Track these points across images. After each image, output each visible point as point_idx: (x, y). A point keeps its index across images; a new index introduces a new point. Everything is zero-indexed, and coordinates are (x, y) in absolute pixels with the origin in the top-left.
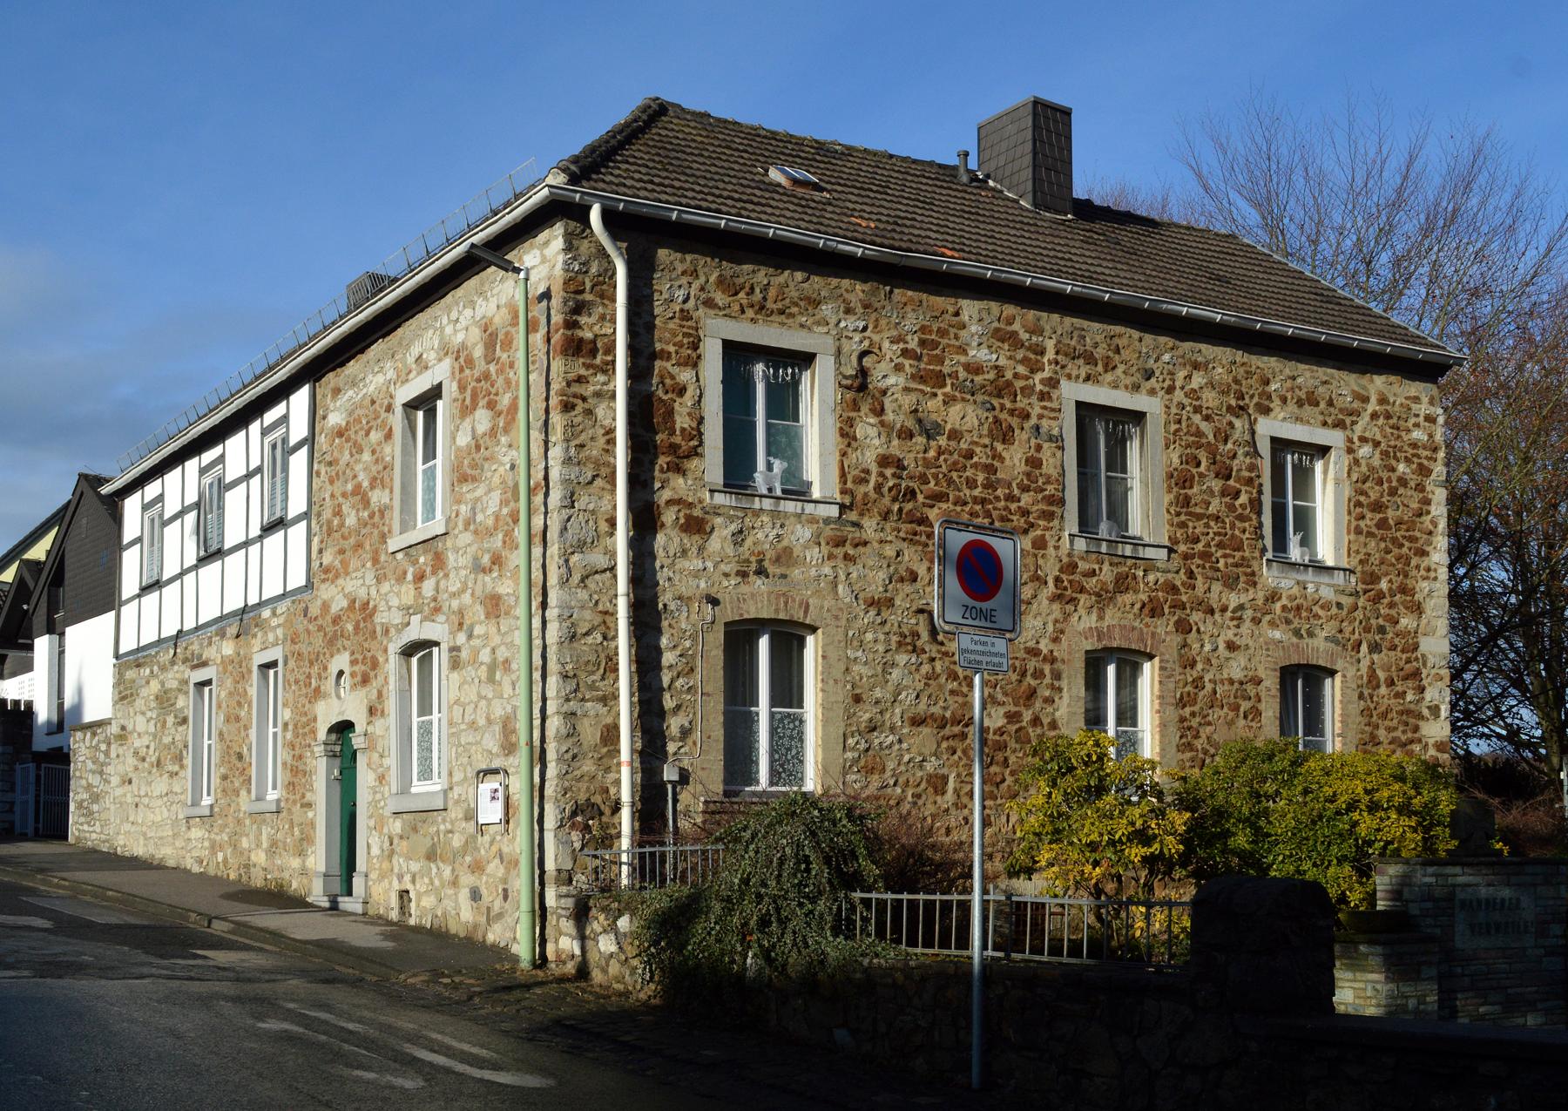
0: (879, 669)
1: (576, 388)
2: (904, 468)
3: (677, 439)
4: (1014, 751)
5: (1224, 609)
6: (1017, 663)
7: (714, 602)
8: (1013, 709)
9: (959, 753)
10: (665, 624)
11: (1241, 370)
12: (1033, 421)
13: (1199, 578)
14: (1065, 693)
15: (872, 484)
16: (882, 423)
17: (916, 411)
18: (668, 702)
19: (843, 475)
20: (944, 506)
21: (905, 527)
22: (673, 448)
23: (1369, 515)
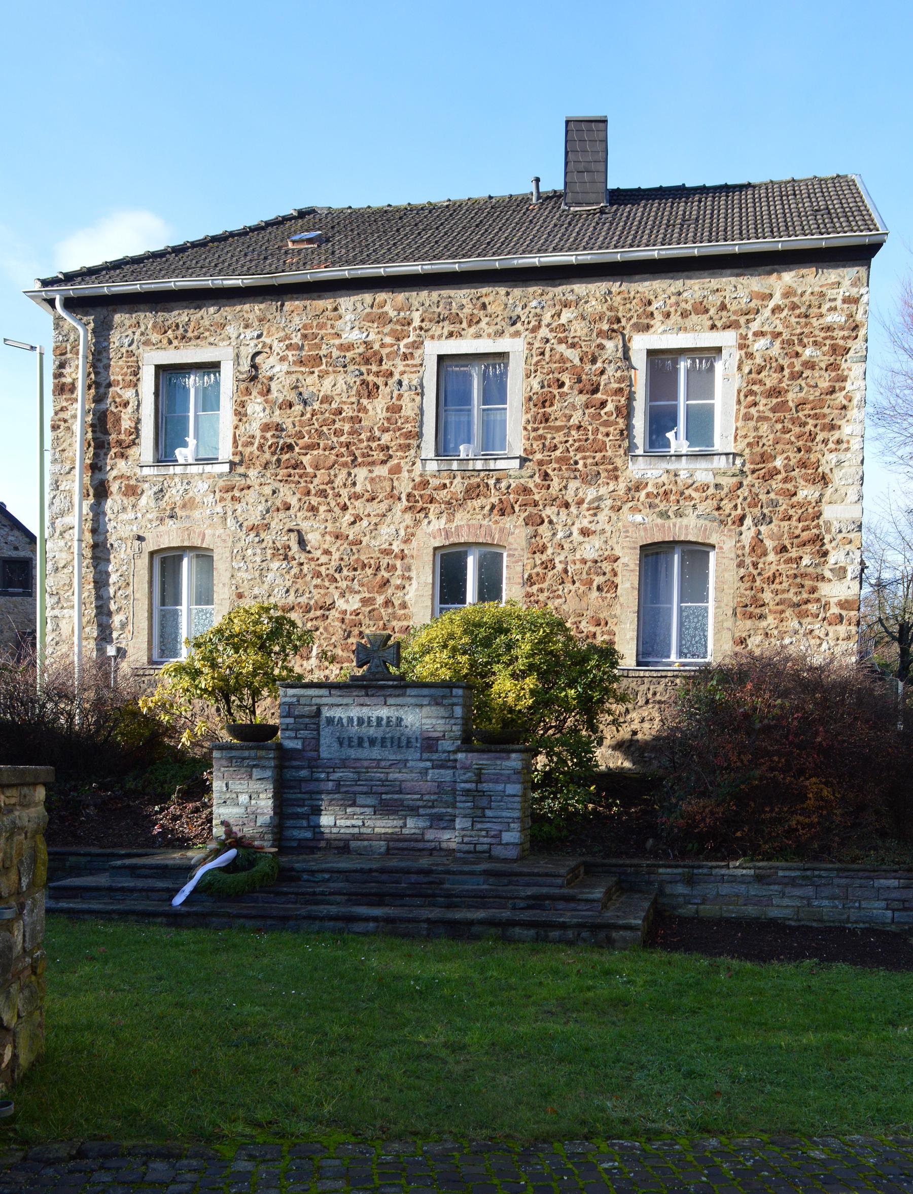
0: (257, 574)
1: (62, 415)
2: (282, 430)
3: (122, 437)
4: (369, 626)
5: (580, 503)
6: (372, 562)
7: (140, 538)
8: (367, 595)
9: (321, 630)
10: (112, 556)
11: (619, 299)
12: (396, 377)
13: (556, 479)
14: (414, 582)
15: (256, 445)
16: (266, 401)
17: (296, 387)
18: (113, 607)
19: (235, 441)
20: (315, 452)
21: (282, 472)
22: (119, 443)
23: (764, 401)
